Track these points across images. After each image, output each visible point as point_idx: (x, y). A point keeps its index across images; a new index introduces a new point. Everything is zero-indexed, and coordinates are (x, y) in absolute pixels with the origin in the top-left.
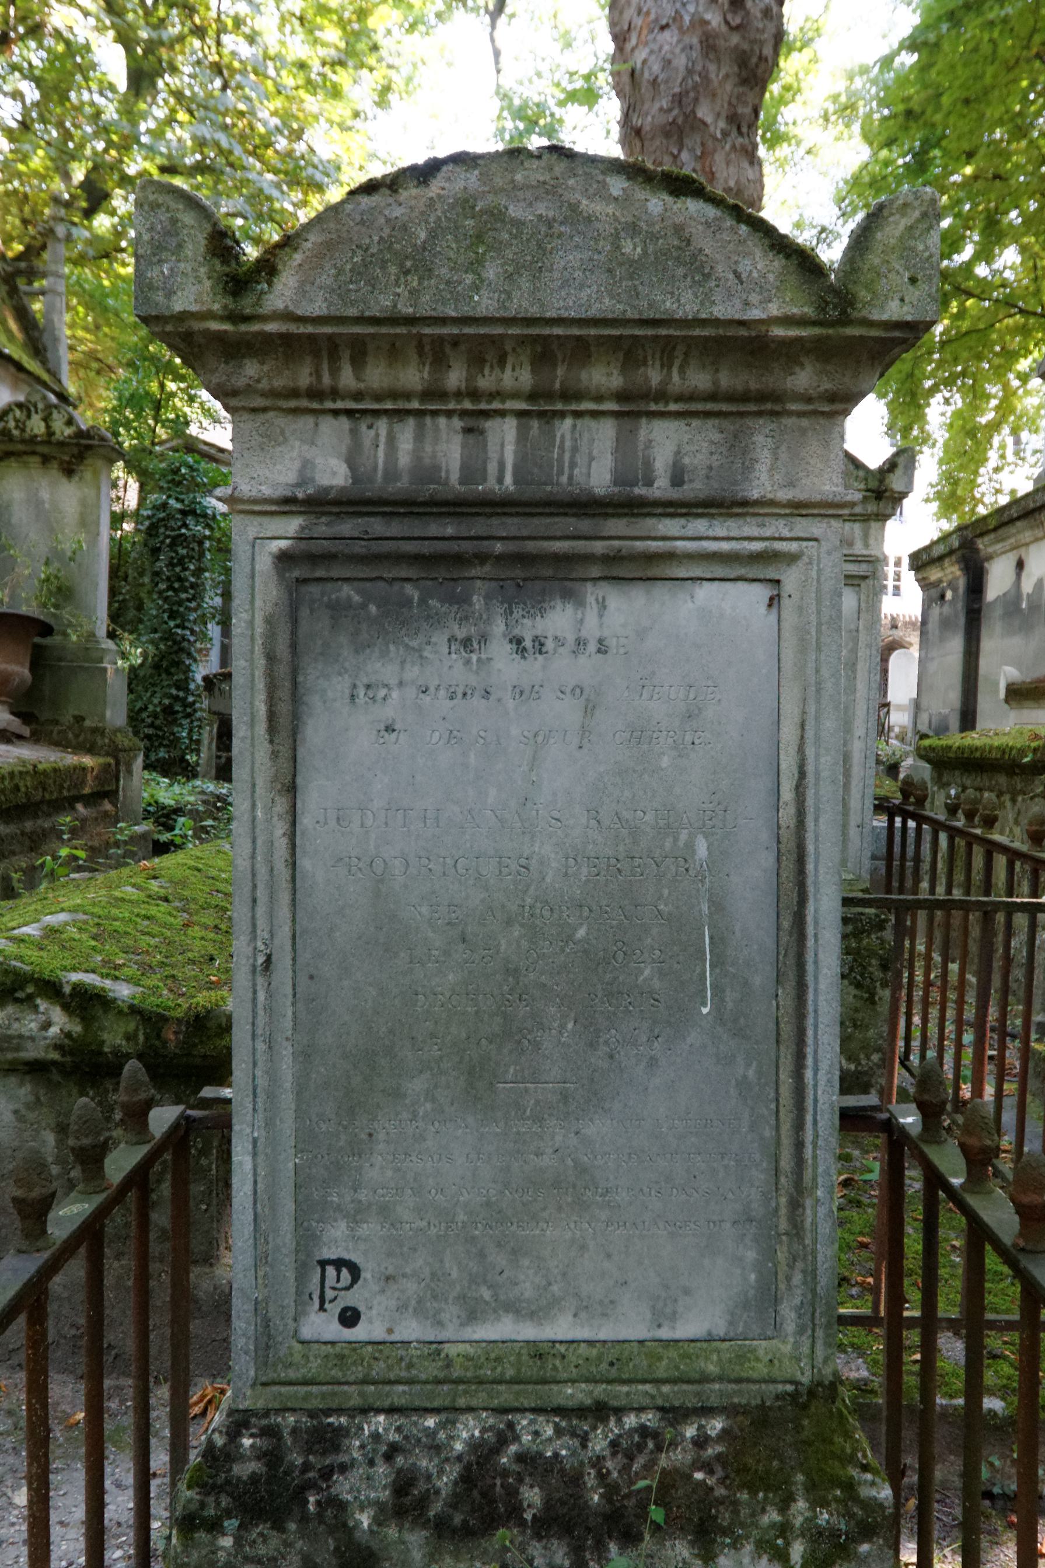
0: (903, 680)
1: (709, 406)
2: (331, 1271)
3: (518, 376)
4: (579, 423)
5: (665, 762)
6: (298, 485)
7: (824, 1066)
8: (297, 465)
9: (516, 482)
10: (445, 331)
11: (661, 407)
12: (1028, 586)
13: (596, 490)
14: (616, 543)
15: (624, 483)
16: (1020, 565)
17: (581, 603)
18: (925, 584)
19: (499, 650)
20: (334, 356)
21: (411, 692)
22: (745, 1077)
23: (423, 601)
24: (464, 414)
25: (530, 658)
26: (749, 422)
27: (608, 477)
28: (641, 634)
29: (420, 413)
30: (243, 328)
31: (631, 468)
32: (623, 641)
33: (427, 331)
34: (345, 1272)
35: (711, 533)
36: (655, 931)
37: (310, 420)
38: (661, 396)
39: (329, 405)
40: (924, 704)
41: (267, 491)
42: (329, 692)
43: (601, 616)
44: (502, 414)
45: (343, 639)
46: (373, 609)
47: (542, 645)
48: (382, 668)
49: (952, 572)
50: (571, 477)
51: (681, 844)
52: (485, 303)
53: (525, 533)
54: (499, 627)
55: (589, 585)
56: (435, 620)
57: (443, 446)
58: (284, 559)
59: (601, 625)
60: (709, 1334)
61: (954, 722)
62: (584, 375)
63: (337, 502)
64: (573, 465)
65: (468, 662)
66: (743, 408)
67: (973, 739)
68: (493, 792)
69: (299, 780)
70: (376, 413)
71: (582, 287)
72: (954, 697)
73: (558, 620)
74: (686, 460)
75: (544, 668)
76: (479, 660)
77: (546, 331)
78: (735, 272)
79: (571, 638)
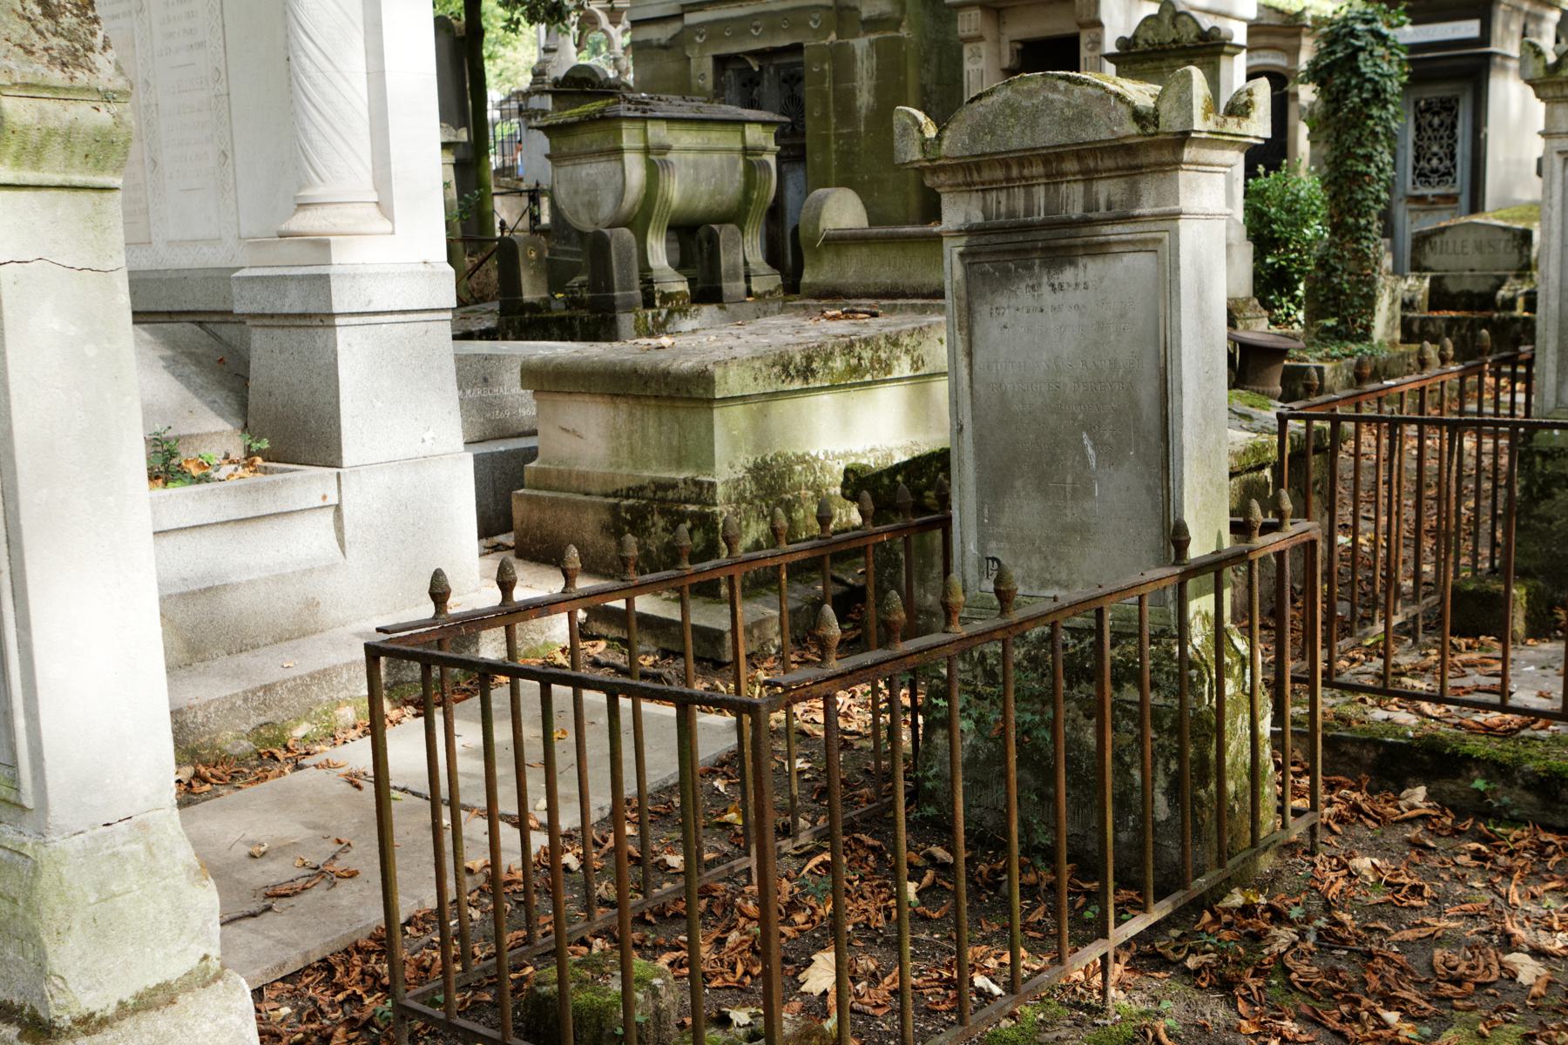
3: (1038, 170)
19: (1046, 289)
20: (970, 170)
28: (1101, 279)
48: (1002, 301)
52: (1015, 144)
54: (1045, 280)
56: (1021, 278)
73: (1068, 275)
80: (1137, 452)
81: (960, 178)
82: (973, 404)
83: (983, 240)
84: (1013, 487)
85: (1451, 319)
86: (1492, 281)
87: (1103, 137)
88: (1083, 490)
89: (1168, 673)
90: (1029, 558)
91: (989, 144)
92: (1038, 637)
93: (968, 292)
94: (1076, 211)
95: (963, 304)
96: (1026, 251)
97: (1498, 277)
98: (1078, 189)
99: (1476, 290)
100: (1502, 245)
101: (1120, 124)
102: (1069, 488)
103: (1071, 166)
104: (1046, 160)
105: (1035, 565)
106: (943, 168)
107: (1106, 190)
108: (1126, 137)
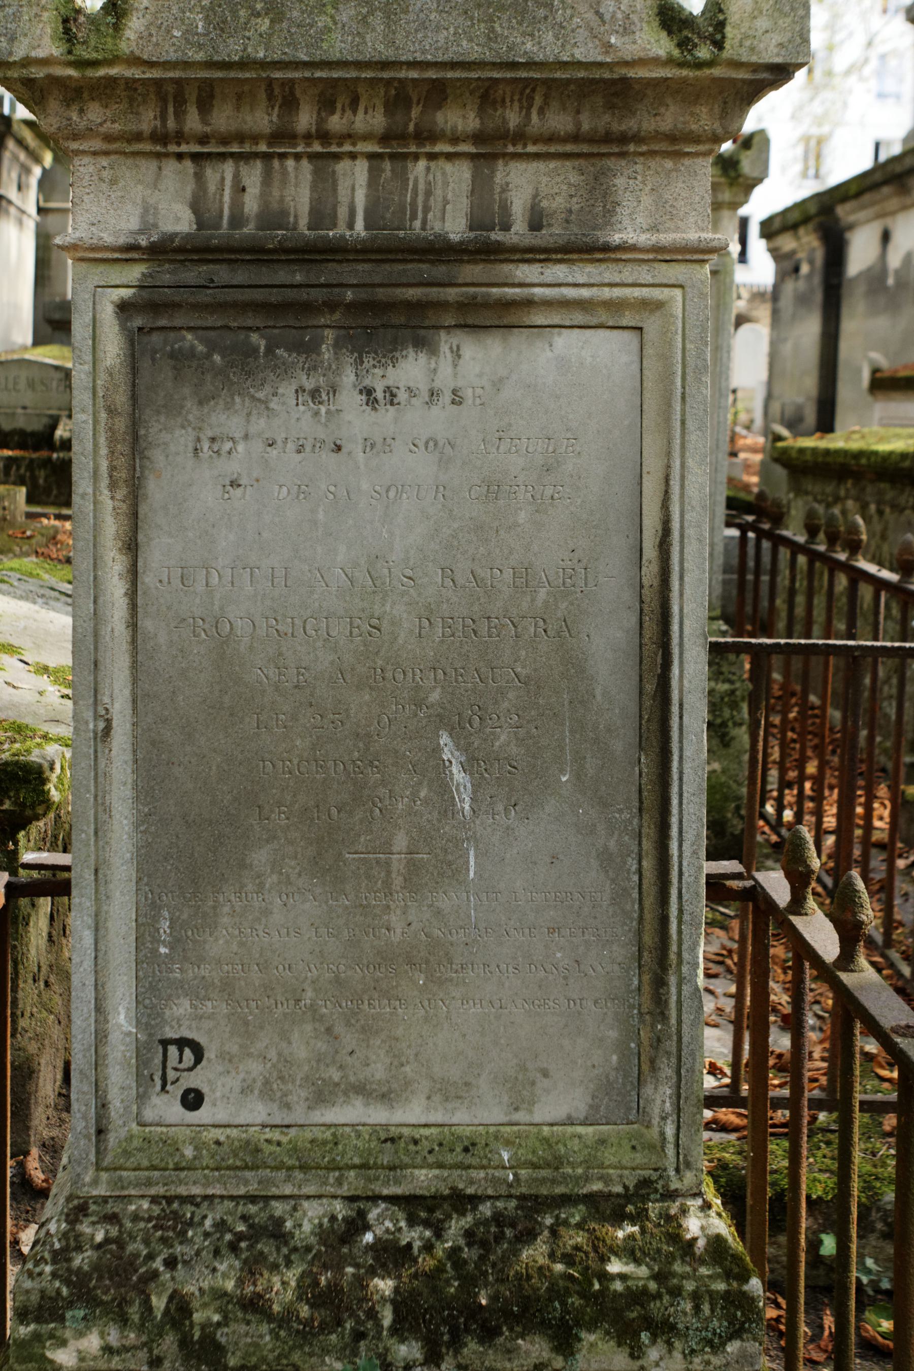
0: (749, 360)
1: (569, 148)
2: (173, 1050)
3: (371, 119)
4: (433, 164)
5: (522, 517)
6: (141, 232)
7: (689, 836)
8: (138, 211)
9: (367, 228)
10: (297, 75)
11: (519, 149)
12: (895, 260)
13: (452, 236)
14: (472, 290)
15: (481, 227)
16: (886, 237)
17: (433, 351)
18: (775, 253)
19: (349, 399)
20: (180, 102)
21: (258, 446)
22: (606, 848)
23: (270, 350)
24: (313, 157)
25: (382, 409)
26: (611, 163)
27: (464, 221)
28: (498, 384)
29: (267, 157)
30: (90, 73)
31: (487, 214)
32: (479, 391)
33: (278, 75)
34: (187, 1052)
35: (570, 280)
36: (511, 695)
37: (153, 164)
38: (520, 136)
39: (172, 148)
40: (776, 392)
41: (109, 239)
42: (172, 444)
43: (455, 366)
44: (353, 156)
45: (187, 391)
46: (217, 358)
47: (393, 395)
48: (227, 420)
49: (807, 245)
50: (424, 222)
51: (539, 603)
52: (338, 46)
53: (377, 280)
54: (348, 377)
55: (443, 334)
56: (286, 371)
57: (290, 191)
58: (123, 307)
59: (455, 375)
60: (569, 1117)
61: (810, 417)
62: (440, 117)
63: (180, 250)
64: (427, 209)
65: (317, 414)
66: (604, 149)
67: (836, 442)
68: (342, 549)
69: (140, 537)
70: (222, 156)
71: (438, 29)
72: (810, 384)
73: (410, 370)
74: (544, 204)
75: (396, 420)
76: (328, 412)
77: (402, 74)
78: (597, 13)
79: (424, 388)
80: (578, 776)
81: (148, 120)
82: (135, 665)
83: (192, 275)
84: (243, 865)
85: (9, 458)
86: (45, 421)
87: (580, 54)
88: (435, 864)
89: (696, 1297)
90: (285, 1036)
91: (266, 39)
92: (322, 1233)
93: (134, 398)
94: (455, 227)
95: (121, 424)
96: (307, 308)
97: (51, 416)
98: (458, 176)
99: (29, 429)
100: (54, 384)
101: (627, 30)
102: (398, 862)
103: (459, 118)
104: (398, 97)
105: (300, 1051)
106: (105, 90)
107: (528, 185)
108: (641, 62)
